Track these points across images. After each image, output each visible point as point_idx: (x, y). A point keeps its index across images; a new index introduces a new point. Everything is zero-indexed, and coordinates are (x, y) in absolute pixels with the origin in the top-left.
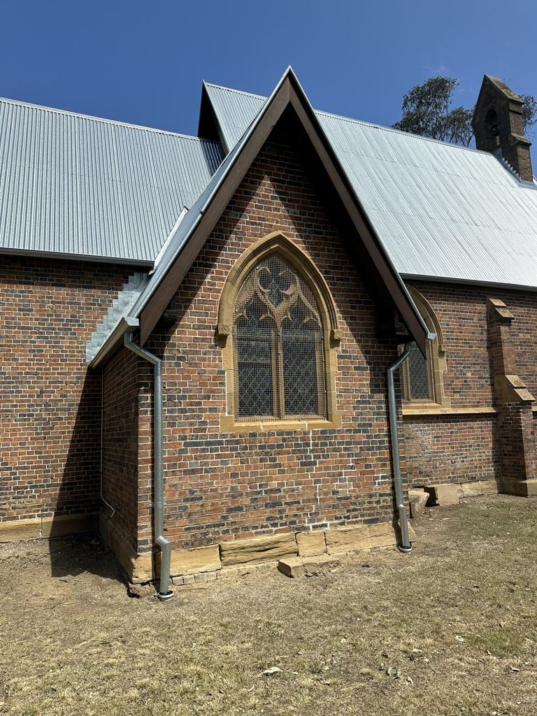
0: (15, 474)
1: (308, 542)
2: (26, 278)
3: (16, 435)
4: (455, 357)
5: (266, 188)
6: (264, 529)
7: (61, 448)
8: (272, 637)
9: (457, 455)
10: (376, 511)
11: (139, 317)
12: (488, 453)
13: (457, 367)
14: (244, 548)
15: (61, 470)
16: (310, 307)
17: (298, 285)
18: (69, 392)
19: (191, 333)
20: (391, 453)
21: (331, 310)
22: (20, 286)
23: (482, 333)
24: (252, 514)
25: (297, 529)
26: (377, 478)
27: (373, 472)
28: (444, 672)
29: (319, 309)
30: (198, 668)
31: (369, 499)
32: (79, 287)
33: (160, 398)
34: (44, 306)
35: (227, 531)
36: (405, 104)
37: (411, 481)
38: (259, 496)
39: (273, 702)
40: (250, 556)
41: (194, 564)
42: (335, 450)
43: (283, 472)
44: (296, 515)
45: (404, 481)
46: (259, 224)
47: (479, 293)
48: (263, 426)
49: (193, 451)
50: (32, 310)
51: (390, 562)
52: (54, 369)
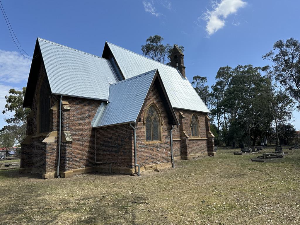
0: (76, 156)
2: (77, 103)
7: (86, 150)
20: (171, 148)
21: (161, 118)
29: (159, 118)
32: (90, 106)
35: (145, 164)
36: (147, 41)
42: (162, 148)
43: (154, 152)
49: (140, 148)
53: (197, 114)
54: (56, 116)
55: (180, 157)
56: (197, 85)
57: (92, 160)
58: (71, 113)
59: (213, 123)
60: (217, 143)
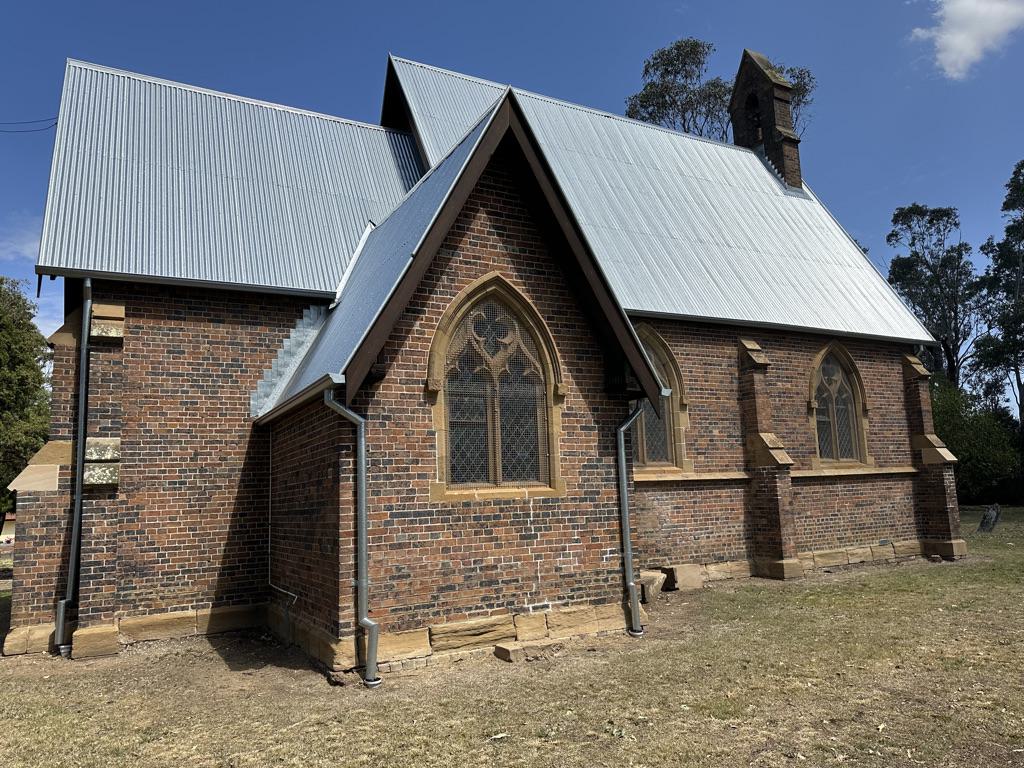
0: (164, 555)
1: (528, 625)
2: (176, 312)
3: (164, 507)
4: (700, 410)
5: (481, 222)
6: (478, 611)
7: (220, 524)
8: (496, 713)
9: (701, 529)
10: (603, 590)
11: (344, 373)
12: (738, 527)
13: (701, 423)
14: (456, 632)
15: (220, 551)
16: (532, 358)
17: (518, 332)
18: (230, 454)
19: (397, 389)
20: (621, 525)
22: (169, 322)
23: (732, 382)
24: (465, 594)
25: (515, 610)
26: (605, 553)
27: (601, 546)
28: (667, 731)
29: (541, 359)
30: (425, 738)
31: (595, 577)
32: (242, 323)
33: (364, 463)
34: (199, 348)
35: (438, 613)
36: (647, 71)
37: (646, 561)
38: (473, 574)
39: (503, 758)
40: (463, 641)
41: (401, 650)
42: (558, 521)
43: (499, 546)
44: (514, 595)
45: (635, 557)
46: (475, 264)
47: (729, 333)
48: (478, 495)
49: (400, 523)
50: (184, 352)
51: (619, 646)
52: (211, 426)
53: (847, 350)
54: (67, 372)
56: (913, 244)
57: (249, 572)
58: (144, 357)
59: (1003, 404)
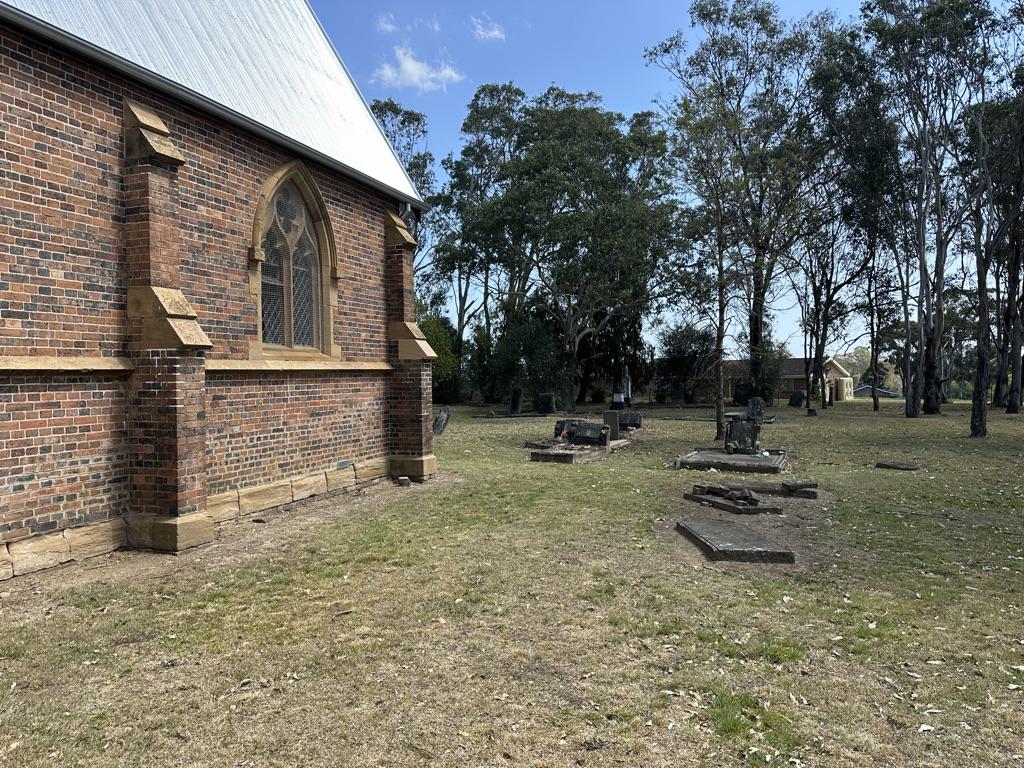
55: (106, 525)
59: (443, 314)
60: (447, 394)
